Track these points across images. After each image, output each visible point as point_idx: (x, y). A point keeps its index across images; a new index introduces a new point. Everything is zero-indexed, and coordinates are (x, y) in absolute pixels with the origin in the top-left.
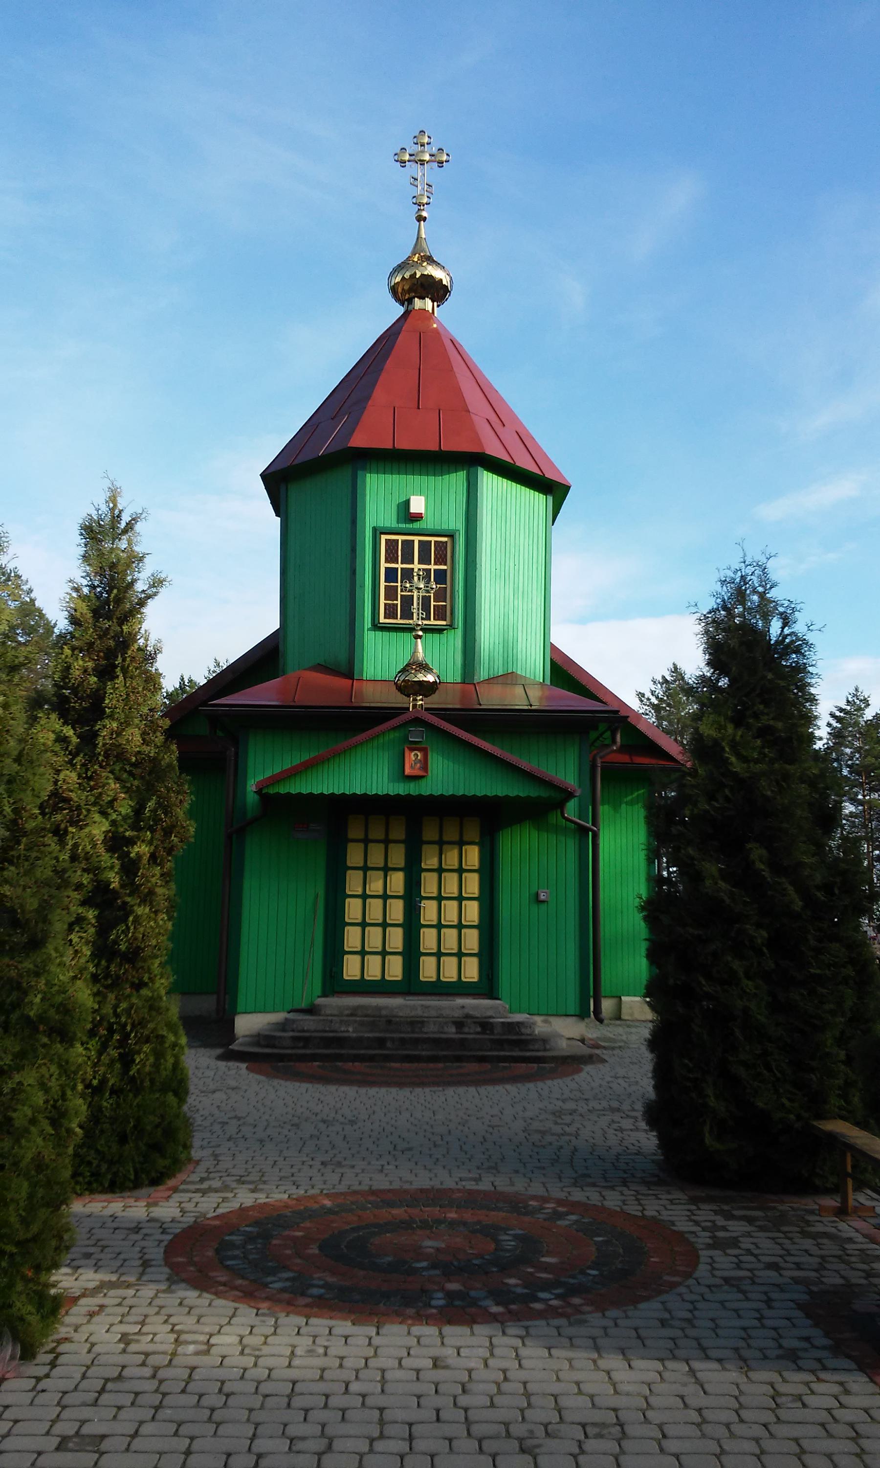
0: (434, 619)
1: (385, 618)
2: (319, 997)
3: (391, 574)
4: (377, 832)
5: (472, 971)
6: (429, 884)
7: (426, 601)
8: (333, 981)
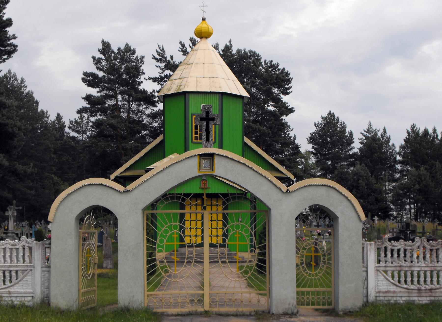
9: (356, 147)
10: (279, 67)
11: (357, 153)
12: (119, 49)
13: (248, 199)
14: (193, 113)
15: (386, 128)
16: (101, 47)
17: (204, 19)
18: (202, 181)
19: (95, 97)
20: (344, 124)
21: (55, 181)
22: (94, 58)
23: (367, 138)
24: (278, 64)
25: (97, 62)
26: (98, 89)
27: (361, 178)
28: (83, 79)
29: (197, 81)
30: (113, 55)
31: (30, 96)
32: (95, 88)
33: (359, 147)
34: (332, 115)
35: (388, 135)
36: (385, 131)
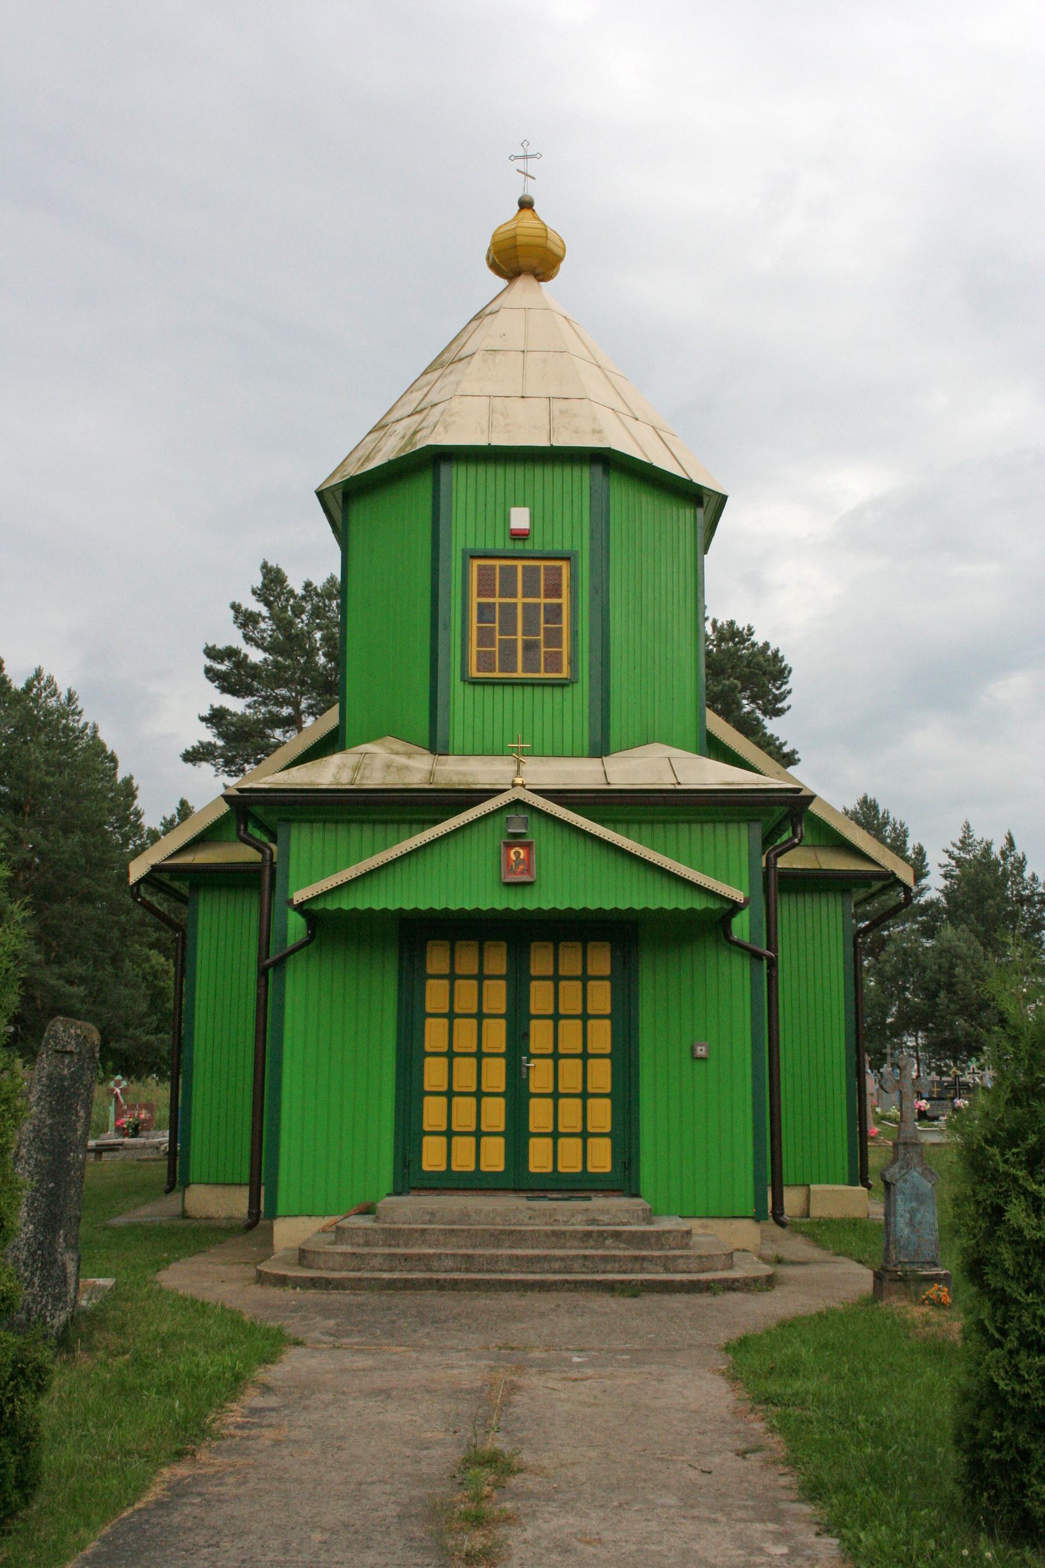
0: (560, 596)
1: (479, 670)
2: (388, 1195)
3: (485, 611)
4: (467, 963)
5: (602, 1158)
6: (540, 997)
7: (530, 647)
8: (409, 1177)
9: (934, 887)
10: (754, 638)
11: (938, 900)
12: (308, 585)
13: (738, 944)
14: (471, 545)
15: (1014, 835)
16: (258, 581)
17: (526, 204)
18: (509, 846)
19: (235, 714)
20: (902, 826)
21: (159, 968)
22: (236, 607)
23: (960, 863)
24: (749, 629)
25: (246, 620)
26: (249, 700)
27: (959, 961)
28: (208, 671)
29: (492, 411)
30: (292, 601)
31: (97, 748)
32: (243, 697)
33: (941, 887)
34: (871, 806)
35: (1019, 851)
36: (1011, 842)
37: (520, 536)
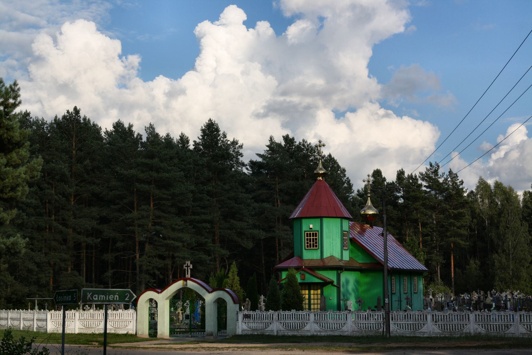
3: (307, 239)
37: (311, 228)
